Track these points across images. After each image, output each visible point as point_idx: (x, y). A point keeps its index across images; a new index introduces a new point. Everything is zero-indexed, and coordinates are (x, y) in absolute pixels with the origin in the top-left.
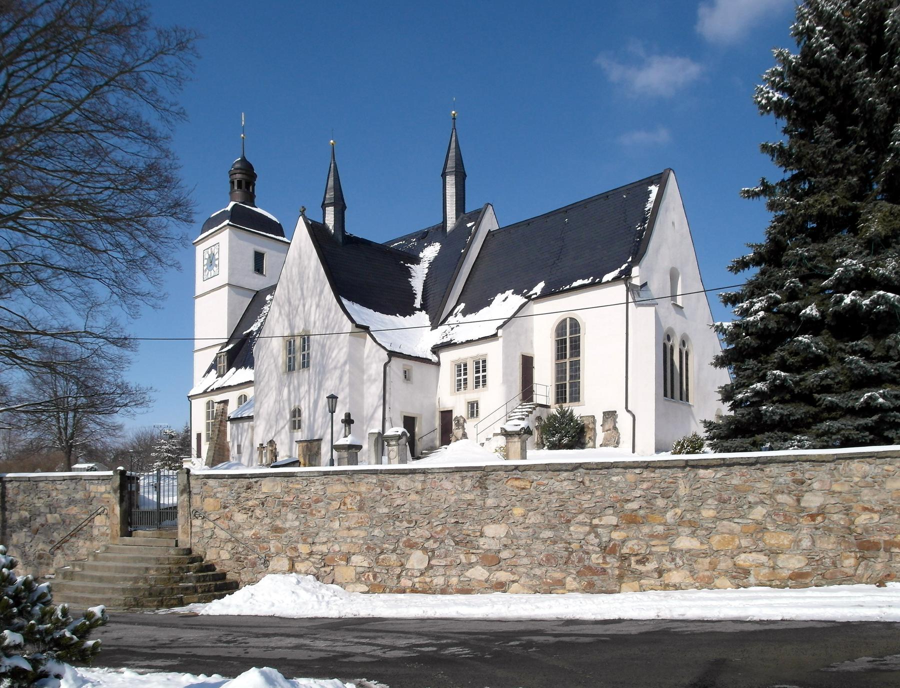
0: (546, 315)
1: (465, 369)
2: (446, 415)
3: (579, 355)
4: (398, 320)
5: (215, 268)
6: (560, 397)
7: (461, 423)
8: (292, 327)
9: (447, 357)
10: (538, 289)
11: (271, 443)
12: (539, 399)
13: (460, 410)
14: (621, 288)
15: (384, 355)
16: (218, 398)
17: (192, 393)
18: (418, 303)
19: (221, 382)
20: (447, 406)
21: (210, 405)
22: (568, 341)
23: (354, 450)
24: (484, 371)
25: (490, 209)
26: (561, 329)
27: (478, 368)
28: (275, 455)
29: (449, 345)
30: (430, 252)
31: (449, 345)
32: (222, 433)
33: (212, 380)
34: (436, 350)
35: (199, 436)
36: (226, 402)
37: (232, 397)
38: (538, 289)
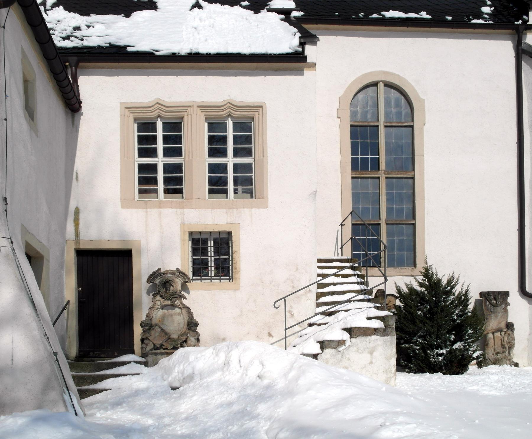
2: (105, 274)
22: (381, 144)
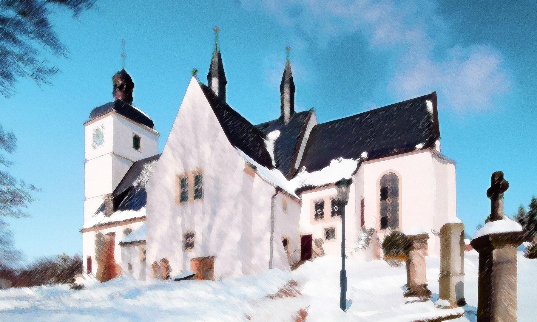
0: (375, 171)
4: (266, 169)
6: (384, 223)
7: (319, 243)
8: (185, 164)
9: (308, 198)
10: (364, 155)
11: (165, 261)
12: (368, 225)
14: (427, 154)
15: (273, 190)
16: (105, 231)
17: (85, 226)
18: (274, 163)
19: (108, 220)
20: (306, 231)
21: (99, 236)
22: (388, 191)
28: (168, 269)
29: (310, 188)
30: (274, 135)
31: (310, 188)
32: (110, 255)
33: (102, 218)
34: (299, 192)
35: (89, 260)
36: (113, 234)
37: (119, 231)
38: (364, 155)
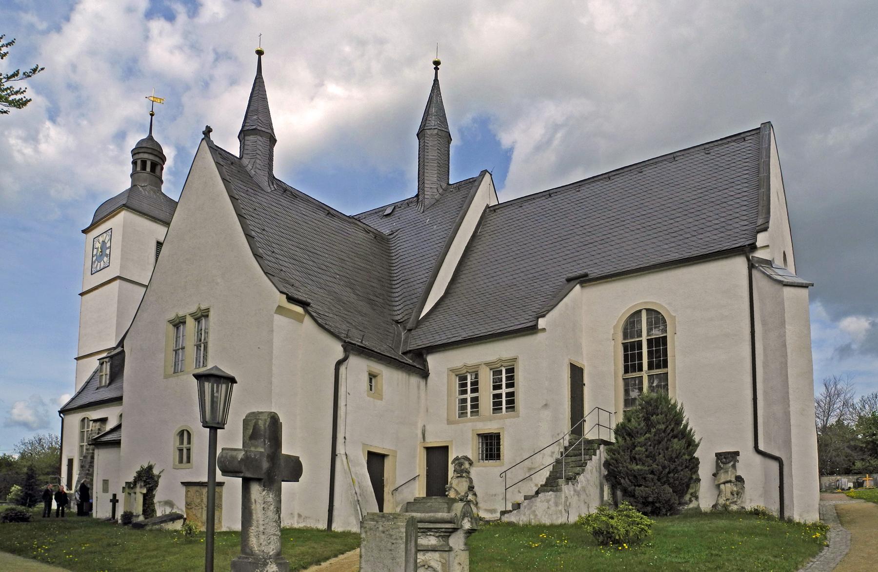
1: (475, 383)
3: (666, 365)
5: (105, 259)
13: (464, 446)
22: (646, 349)
23: (219, 542)
24: (510, 385)
25: (487, 176)
26: (631, 324)
27: (464, 385)
35: (70, 462)
36: (104, 421)
